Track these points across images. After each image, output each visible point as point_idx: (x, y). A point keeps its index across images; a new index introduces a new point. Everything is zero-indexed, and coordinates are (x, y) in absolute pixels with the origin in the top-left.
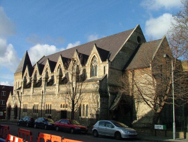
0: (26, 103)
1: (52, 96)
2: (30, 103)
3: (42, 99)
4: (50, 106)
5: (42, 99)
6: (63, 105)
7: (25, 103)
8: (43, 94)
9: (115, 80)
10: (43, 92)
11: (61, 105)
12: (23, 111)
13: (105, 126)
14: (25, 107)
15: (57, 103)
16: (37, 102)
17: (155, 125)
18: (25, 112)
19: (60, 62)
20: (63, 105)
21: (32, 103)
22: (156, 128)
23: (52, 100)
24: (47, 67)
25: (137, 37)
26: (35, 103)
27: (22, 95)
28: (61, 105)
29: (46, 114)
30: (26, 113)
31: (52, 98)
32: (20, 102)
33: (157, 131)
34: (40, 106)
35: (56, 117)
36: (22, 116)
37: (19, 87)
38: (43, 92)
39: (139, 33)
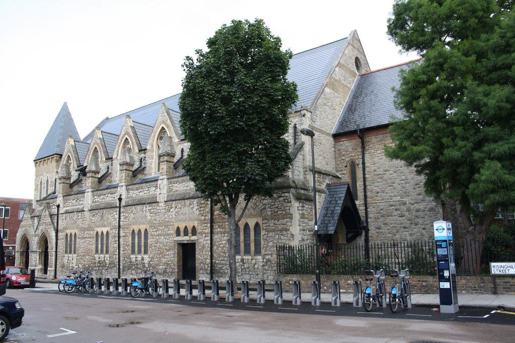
0: (73, 232)
1: (148, 207)
2: (83, 230)
3: (119, 218)
4: (69, 236)
5: (119, 218)
6: (182, 229)
7: (68, 232)
8: (120, 204)
9: (320, 158)
10: (120, 199)
11: (178, 228)
12: (66, 252)
13: (495, 292)
14: (302, 97)
15: (167, 225)
16: (105, 226)
17: (493, 264)
18: (70, 253)
19: (163, 122)
20: (182, 229)
21: (90, 228)
22: (497, 272)
23: (149, 218)
24: (127, 136)
25: (354, 58)
26: (99, 230)
27: (61, 211)
28: (133, 231)
29: (133, 256)
30: (75, 255)
31: (148, 214)
32: (57, 232)
33: (497, 281)
34: (115, 236)
35: (164, 260)
36: (64, 264)
37: (50, 192)
38: (120, 199)
39: (358, 49)
